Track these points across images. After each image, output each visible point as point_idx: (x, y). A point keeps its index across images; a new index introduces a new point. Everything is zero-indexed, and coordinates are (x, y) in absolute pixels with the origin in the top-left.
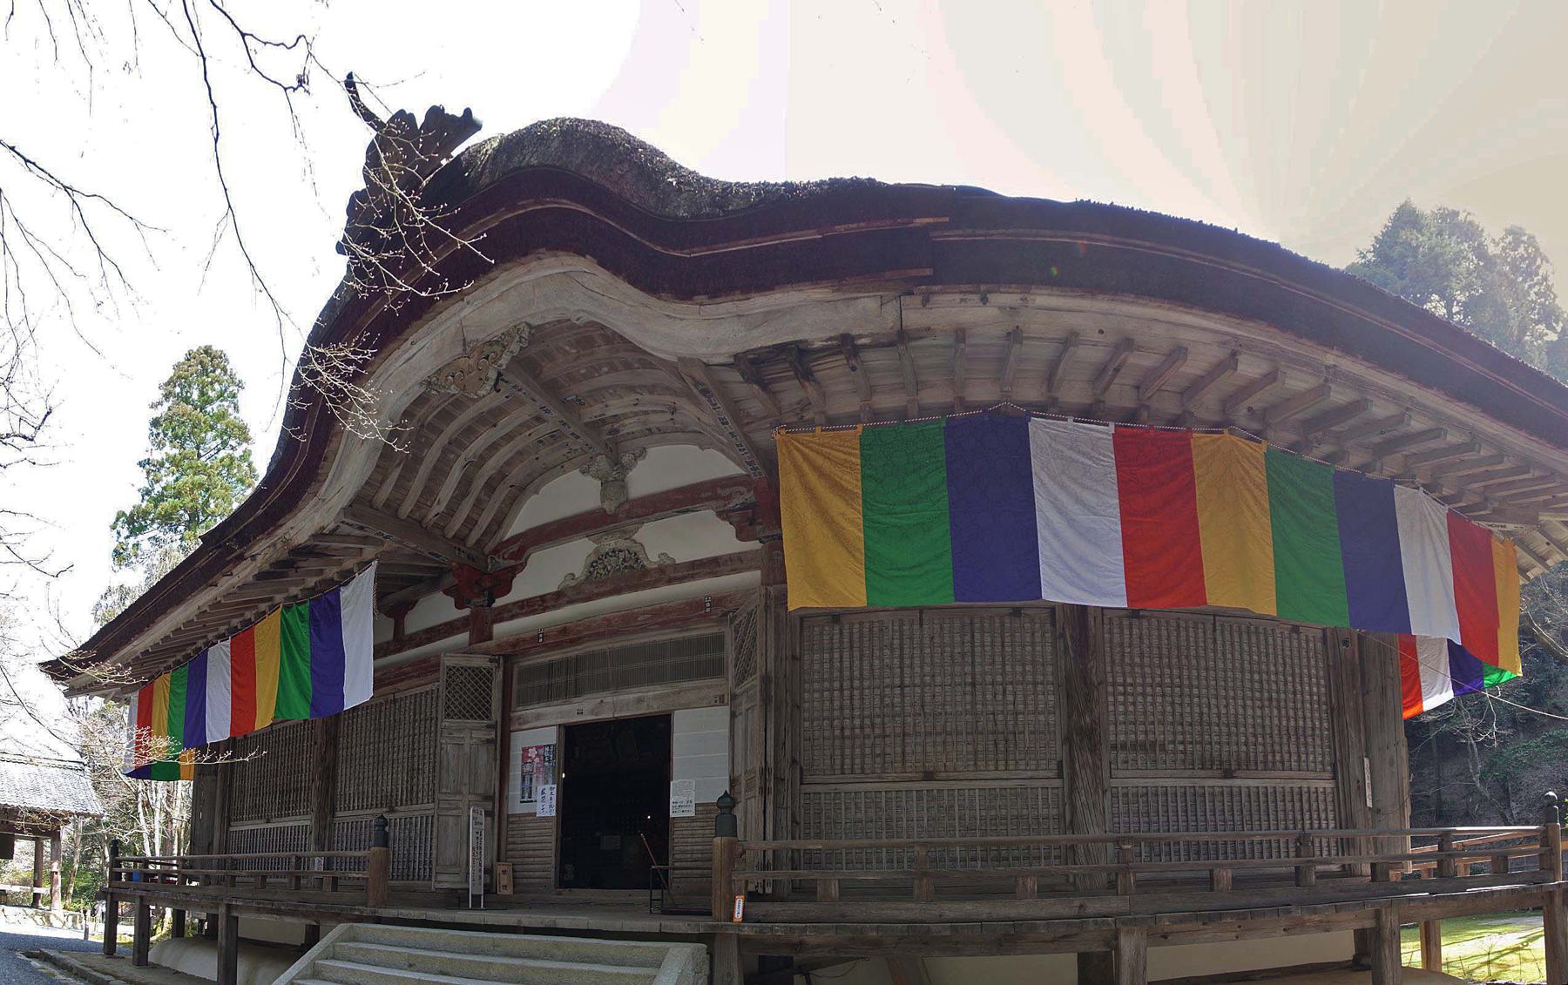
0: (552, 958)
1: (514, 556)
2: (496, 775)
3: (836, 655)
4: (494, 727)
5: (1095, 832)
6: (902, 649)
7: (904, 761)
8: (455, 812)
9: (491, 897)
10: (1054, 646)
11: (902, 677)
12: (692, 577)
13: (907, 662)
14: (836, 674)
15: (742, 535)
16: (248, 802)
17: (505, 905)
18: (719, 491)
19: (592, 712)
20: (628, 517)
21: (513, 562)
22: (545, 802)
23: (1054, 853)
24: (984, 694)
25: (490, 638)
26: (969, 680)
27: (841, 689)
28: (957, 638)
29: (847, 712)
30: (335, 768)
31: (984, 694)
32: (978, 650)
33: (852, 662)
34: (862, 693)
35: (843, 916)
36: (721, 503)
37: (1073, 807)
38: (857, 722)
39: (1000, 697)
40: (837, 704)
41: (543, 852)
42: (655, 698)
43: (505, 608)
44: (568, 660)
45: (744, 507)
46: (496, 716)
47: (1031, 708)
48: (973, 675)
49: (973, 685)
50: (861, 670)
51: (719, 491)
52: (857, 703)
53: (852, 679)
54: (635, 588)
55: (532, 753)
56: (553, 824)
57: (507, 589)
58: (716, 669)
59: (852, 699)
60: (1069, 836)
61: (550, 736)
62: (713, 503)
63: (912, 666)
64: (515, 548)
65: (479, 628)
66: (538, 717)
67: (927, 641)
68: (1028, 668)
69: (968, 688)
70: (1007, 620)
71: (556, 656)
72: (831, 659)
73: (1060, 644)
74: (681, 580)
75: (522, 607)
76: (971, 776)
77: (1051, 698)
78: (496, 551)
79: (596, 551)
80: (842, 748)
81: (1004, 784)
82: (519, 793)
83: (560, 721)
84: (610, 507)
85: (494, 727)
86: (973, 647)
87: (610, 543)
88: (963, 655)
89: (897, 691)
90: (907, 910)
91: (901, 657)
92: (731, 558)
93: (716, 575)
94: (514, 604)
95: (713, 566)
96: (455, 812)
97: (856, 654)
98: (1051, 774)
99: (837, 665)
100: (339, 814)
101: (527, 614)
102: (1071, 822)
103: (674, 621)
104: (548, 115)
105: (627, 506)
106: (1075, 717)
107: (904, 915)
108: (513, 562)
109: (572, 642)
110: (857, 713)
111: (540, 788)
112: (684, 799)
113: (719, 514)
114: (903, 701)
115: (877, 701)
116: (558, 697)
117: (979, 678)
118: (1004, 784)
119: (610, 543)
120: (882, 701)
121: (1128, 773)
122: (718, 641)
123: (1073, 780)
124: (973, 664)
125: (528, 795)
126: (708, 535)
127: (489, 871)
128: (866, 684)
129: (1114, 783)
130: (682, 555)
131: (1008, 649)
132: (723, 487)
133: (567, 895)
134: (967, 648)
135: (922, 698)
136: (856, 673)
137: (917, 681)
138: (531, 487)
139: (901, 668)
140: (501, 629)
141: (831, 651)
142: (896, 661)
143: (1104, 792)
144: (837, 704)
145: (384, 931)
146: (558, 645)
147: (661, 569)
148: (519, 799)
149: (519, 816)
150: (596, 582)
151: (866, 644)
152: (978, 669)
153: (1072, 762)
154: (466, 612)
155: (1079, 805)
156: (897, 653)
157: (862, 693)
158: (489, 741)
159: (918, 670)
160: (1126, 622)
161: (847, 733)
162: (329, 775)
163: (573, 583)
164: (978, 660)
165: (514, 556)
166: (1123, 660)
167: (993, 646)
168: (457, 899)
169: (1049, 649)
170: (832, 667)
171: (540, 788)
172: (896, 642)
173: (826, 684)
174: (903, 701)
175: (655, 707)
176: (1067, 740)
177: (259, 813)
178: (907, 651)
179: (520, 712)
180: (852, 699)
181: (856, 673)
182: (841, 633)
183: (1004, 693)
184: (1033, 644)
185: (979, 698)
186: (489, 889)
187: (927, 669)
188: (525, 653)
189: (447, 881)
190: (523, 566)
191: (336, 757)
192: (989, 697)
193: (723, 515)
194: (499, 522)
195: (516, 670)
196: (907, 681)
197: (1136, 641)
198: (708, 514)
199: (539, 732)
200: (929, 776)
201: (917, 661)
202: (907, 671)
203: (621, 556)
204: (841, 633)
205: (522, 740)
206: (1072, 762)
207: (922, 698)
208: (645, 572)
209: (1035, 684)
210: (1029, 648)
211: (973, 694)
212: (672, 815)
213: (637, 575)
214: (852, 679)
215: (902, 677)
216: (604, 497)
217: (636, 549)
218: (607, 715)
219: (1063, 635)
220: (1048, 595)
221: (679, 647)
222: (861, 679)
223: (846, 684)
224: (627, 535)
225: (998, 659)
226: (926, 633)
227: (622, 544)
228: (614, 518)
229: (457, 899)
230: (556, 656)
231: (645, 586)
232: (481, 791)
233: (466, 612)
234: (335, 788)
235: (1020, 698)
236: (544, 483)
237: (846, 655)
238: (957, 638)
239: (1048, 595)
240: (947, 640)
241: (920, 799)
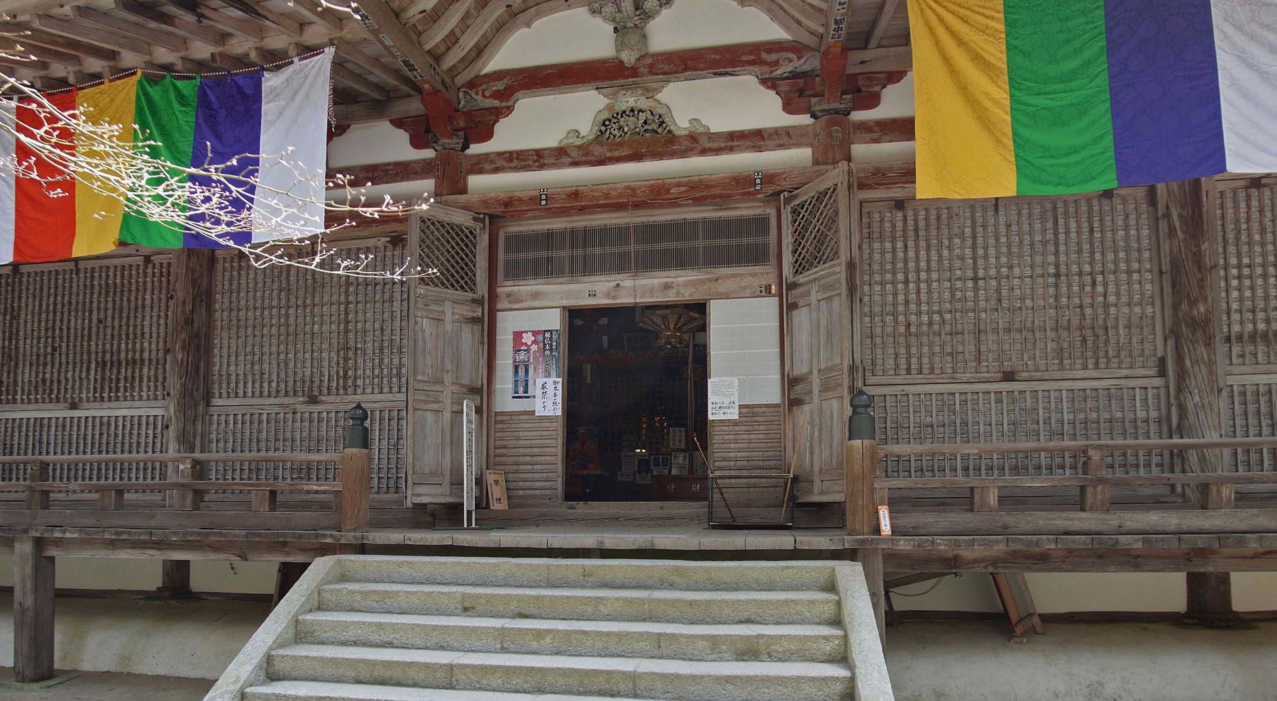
1: (496, 95)
2: (483, 362)
3: (900, 245)
4: (479, 302)
5: (1212, 437)
6: (974, 237)
7: (979, 360)
8: (435, 406)
9: (486, 517)
10: (1155, 229)
11: (975, 269)
12: (731, 150)
13: (981, 252)
14: (900, 265)
15: (788, 107)
16: (26, 374)
17: (502, 522)
18: (764, 55)
19: (608, 295)
20: (651, 73)
21: (496, 103)
22: (548, 397)
23: (1155, 460)
24: (1069, 286)
25: (464, 191)
26: (1052, 270)
27: (906, 282)
28: (1038, 226)
29: (913, 307)
30: (209, 338)
31: (1069, 286)
32: (1062, 237)
33: (917, 252)
34: (929, 287)
35: (1006, 527)
36: (766, 69)
37: (1182, 409)
38: (925, 318)
39: (1088, 289)
40: (901, 298)
41: (547, 461)
42: (686, 284)
43: (485, 157)
44: (573, 232)
45: (794, 75)
46: (482, 289)
47: (1124, 299)
48: (1057, 266)
49: (1057, 275)
50: (928, 261)
51: (764, 55)
52: (924, 297)
53: (918, 271)
55: (528, 339)
56: (559, 427)
57: (487, 135)
58: (757, 255)
59: (918, 292)
60: (1176, 440)
61: (553, 321)
62: (756, 69)
63: (986, 256)
64: (500, 86)
65: (451, 179)
66: (535, 295)
67: (1003, 229)
68: (1122, 255)
69: (1051, 280)
70: (1095, 203)
71: (557, 224)
72: (894, 249)
73: (1163, 226)
74: (718, 151)
75: (510, 160)
76: (1057, 375)
77: (1148, 287)
78: (472, 84)
79: (609, 108)
80: (908, 347)
81: (1096, 384)
82: (510, 386)
83: (565, 303)
84: (628, 57)
85: (479, 302)
86: (1056, 234)
87: (629, 100)
88: (1044, 243)
89: (970, 284)
90: (1080, 519)
91: (974, 247)
93: (759, 149)
94: (500, 154)
95: (756, 139)
96: (435, 406)
97: (922, 244)
98: (1151, 373)
99: (900, 255)
100: (216, 401)
101: (516, 169)
102: (1179, 426)
103: (714, 197)
105: (649, 61)
106: (1184, 306)
107: (1086, 526)
108: (496, 103)
109: (582, 210)
110: (924, 308)
111: (540, 382)
112: (727, 401)
113: (764, 82)
114: (976, 295)
115: (947, 295)
116: (560, 273)
117: (1063, 269)
118: (1096, 384)
119: (629, 100)
120: (953, 295)
121: (1245, 369)
122: (761, 224)
123: (1182, 375)
124: (1057, 253)
125: (522, 390)
126: (749, 104)
127: (479, 481)
128: (935, 276)
129: (1231, 380)
130: (719, 124)
131: (1097, 235)
132: (769, 51)
133: (582, 508)
134: (1050, 236)
135: (998, 291)
136: (923, 265)
137: (992, 272)
138: (522, 17)
139: (974, 259)
140: (477, 182)
141: (893, 241)
142: (968, 252)
143: (1220, 391)
144: (901, 298)
145: (399, 565)
146: (564, 212)
147: (693, 138)
148: (511, 393)
149: (511, 414)
150: (609, 143)
151: (934, 233)
152: (1063, 258)
153: (1179, 359)
154: (428, 154)
155: (1190, 406)
156: (969, 242)
157: (929, 287)
158: (474, 320)
159: (993, 260)
160: (1242, 195)
161: (913, 329)
162: (198, 346)
163: (578, 142)
164: (1062, 248)
165: (496, 95)
166: (1237, 239)
167: (1078, 233)
168: (450, 515)
169: (1145, 232)
170: (894, 256)
171: (540, 382)
172: (968, 231)
173: (889, 277)
174: (976, 295)
175: (687, 295)
176: (1174, 333)
177: (47, 391)
178: (980, 240)
179: (505, 289)
180: (918, 292)
181: (923, 265)
182: (905, 221)
183: (1094, 283)
184: (1126, 228)
185: (1064, 290)
186: (482, 502)
187: (1004, 260)
188: (519, 216)
189: (430, 495)
190: (510, 110)
191: (210, 324)
192: (1076, 289)
193: (769, 83)
194: (480, 51)
195: (502, 235)
196: (981, 273)
197: (1255, 215)
198: (747, 81)
199: (536, 310)
200: (1009, 377)
201: (992, 251)
202: (981, 262)
203: (642, 117)
204: (905, 221)
205: (508, 323)
207: (998, 291)
208: (672, 138)
209: (1129, 272)
210: (1121, 233)
211: (1056, 286)
212: (710, 417)
213: (660, 140)
214: (918, 271)
215: (975, 269)
216: (620, 46)
217: (659, 110)
218: (625, 300)
219: (1167, 216)
221: (715, 227)
222: (929, 270)
223: (912, 276)
224: (650, 93)
225: (1086, 247)
226: (1002, 219)
227: (643, 103)
228: (634, 72)
229: (450, 515)
230: (557, 224)
231: (673, 155)
232: (465, 381)
233: (428, 154)
234: (209, 364)
235: (1111, 288)
236: (539, 15)
237: (911, 244)
238: (1038, 226)
240: (1026, 228)
241: (999, 401)
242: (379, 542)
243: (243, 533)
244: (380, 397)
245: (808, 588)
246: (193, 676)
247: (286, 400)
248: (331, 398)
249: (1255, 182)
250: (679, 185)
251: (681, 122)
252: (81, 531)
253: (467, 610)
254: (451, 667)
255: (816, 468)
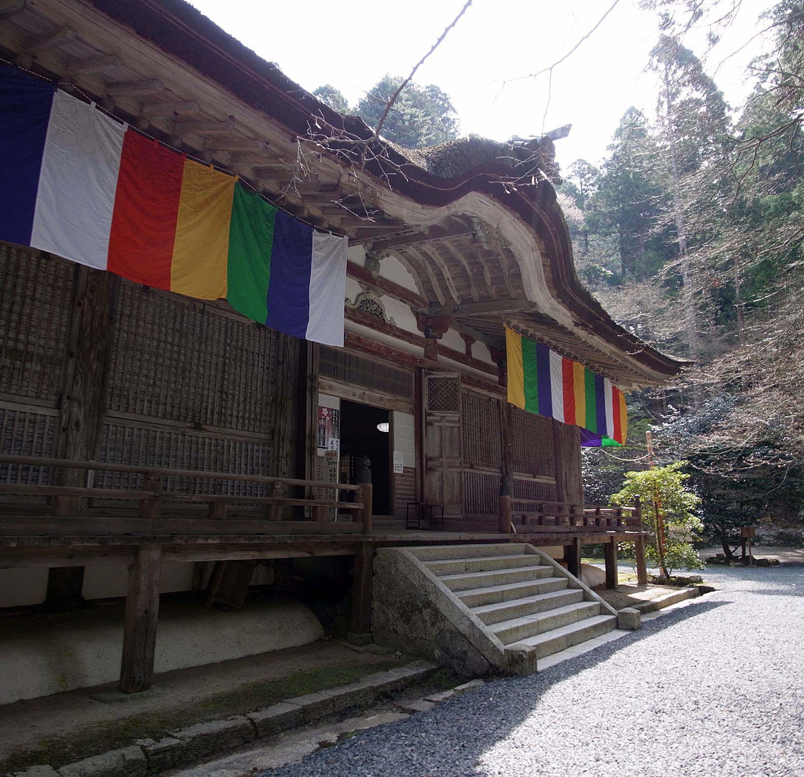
0: (496, 555)
12: (402, 338)
19: (360, 397)
54: (371, 326)
66: (331, 387)
83: (343, 396)
92: (410, 335)
104: (556, 151)
145: (425, 551)
153: (506, 467)
171: (331, 439)
175: (387, 406)
193: (417, 315)
206: (506, 467)
220: (40, 241)
231: (380, 330)
239: (40, 241)
242: (392, 539)
243: (330, 536)
244: (244, 433)
245: (519, 554)
246: (203, 663)
247: (176, 423)
248: (211, 428)
249: (45, 255)
250: (395, 351)
251: (388, 315)
252: (220, 538)
253: (467, 570)
254: (503, 592)
255: (445, 501)
